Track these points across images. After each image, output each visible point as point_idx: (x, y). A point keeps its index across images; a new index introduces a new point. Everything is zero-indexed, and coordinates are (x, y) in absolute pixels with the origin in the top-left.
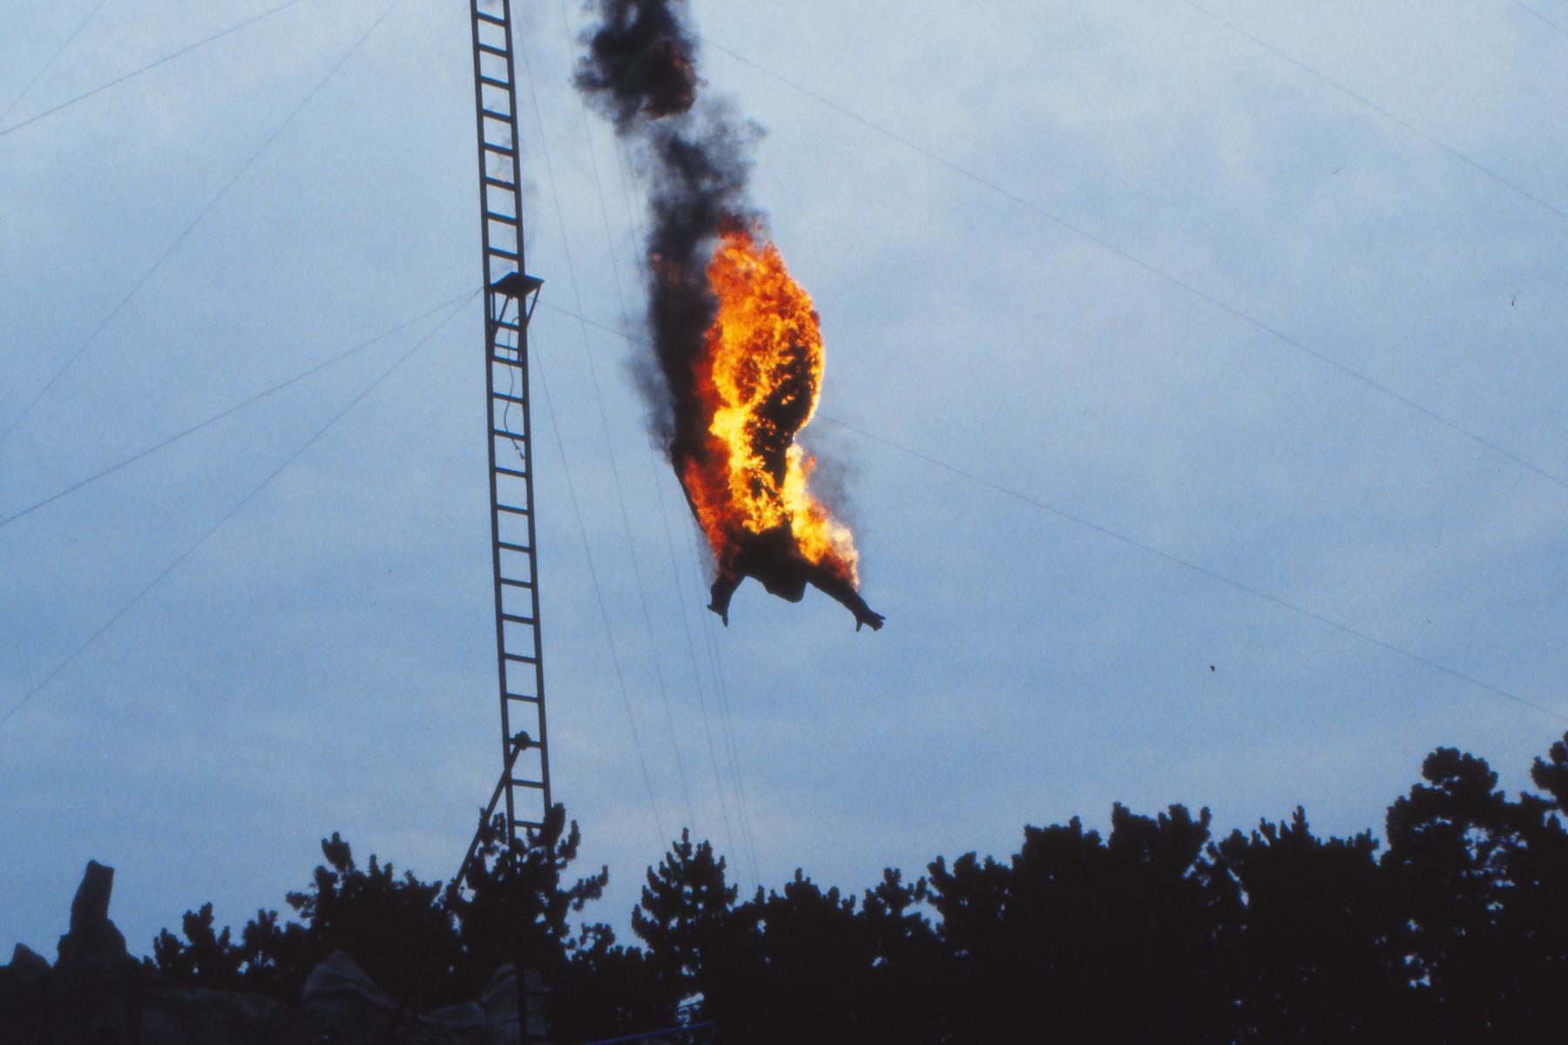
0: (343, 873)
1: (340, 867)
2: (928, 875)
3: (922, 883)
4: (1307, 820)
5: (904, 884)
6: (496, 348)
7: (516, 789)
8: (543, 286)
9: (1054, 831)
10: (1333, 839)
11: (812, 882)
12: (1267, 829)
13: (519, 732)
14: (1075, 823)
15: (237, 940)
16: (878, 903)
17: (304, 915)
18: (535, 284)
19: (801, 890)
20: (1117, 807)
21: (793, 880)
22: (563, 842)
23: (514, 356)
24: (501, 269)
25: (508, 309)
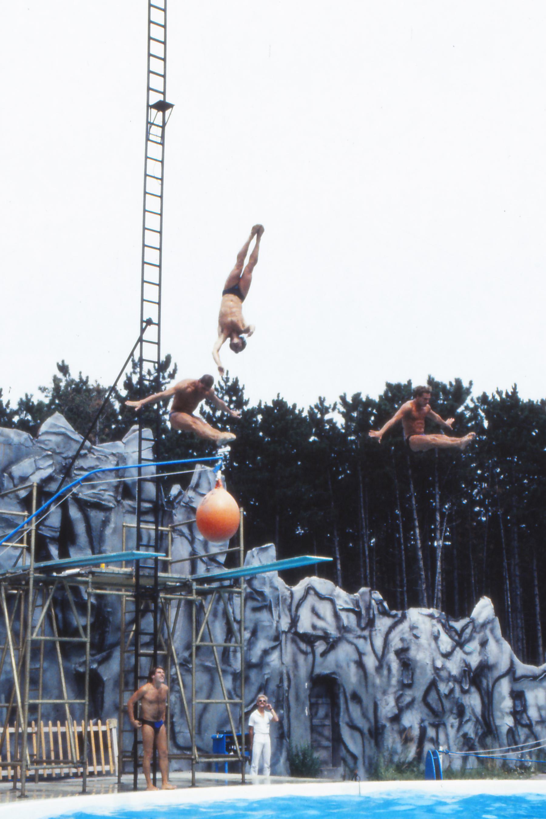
0: (65, 378)
1: (65, 375)
2: (339, 401)
3: (335, 405)
4: (517, 390)
5: (326, 404)
6: (150, 135)
7: (144, 343)
8: (174, 107)
9: (398, 386)
10: (530, 401)
11: (284, 400)
12: (499, 393)
13: (148, 318)
14: (410, 383)
15: (14, 406)
16: (314, 413)
17: (46, 396)
18: (170, 106)
19: (279, 404)
20: (430, 377)
21: (276, 399)
22: (170, 372)
23: (159, 140)
24: (155, 98)
25: (157, 116)
